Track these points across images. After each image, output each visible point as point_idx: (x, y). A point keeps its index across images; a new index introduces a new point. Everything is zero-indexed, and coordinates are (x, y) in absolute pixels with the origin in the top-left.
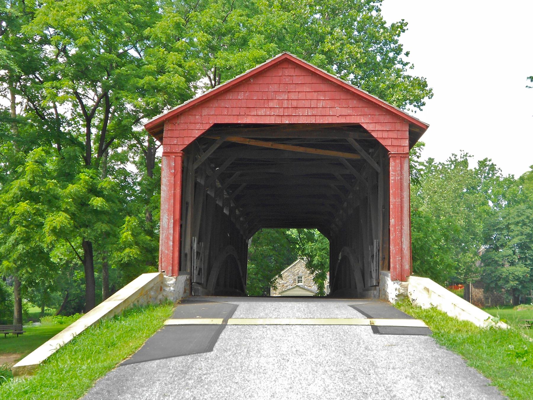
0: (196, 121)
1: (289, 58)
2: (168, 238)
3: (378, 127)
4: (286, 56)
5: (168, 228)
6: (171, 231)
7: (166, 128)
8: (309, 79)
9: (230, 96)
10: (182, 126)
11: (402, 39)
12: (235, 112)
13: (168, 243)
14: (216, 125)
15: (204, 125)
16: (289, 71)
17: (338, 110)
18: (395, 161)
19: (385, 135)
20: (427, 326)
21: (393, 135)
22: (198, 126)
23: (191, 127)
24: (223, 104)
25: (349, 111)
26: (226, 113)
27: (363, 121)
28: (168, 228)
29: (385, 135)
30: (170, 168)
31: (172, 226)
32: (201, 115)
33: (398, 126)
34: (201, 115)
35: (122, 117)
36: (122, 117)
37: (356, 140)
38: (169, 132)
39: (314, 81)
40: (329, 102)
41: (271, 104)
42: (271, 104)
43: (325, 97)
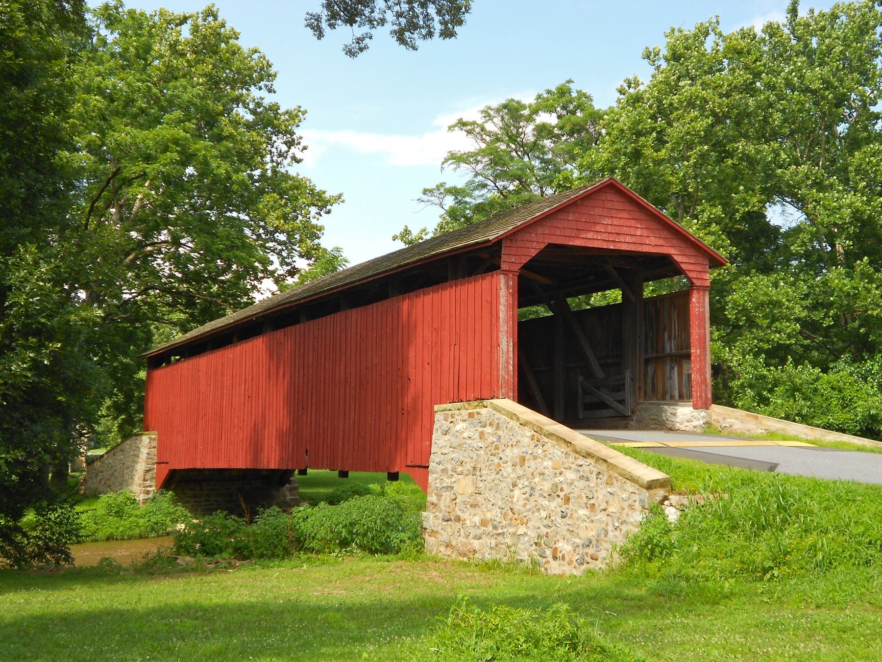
0: (532, 240)
1: (614, 182)
2: (507, 362)
3: (685, 260)
4: (612, 181)
5: (508, 351)
6: (511, 355)
7: (503, 242)
8: (627, 206)
9: (561, 216)
10: (520, 244)
11: (348, 25)
12: (568, 233)
13: (507, 367)
14: (549, 244)
15: (540, 244)
16: (611, 196)
17: (654, 241)
18: (698, 293)
19: (691, 267)
20: (667, 476)
21: (698, 268)
22: (534, 245)
23: (528, 245)
24: (555, 224)
25: (661, 242)
26: (558, 233)
27: (674, 252)
28: (508, 351)
29: (691, 267)
30: (508, 288)
31: (511, 349)
32: (536, 234)
33: (701, 260)
34: (536, 234)
35: (227, 197)
36: (227, 197)
37: (615, 268)
38: (507, 248)
39: (631, 208)
40: (645, 231)
41: (598, 228)
42: (598, 228)
43: (641, 225)
